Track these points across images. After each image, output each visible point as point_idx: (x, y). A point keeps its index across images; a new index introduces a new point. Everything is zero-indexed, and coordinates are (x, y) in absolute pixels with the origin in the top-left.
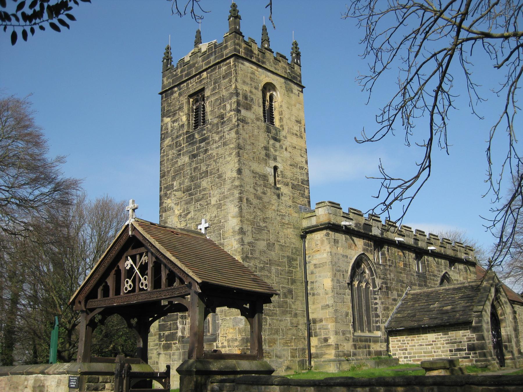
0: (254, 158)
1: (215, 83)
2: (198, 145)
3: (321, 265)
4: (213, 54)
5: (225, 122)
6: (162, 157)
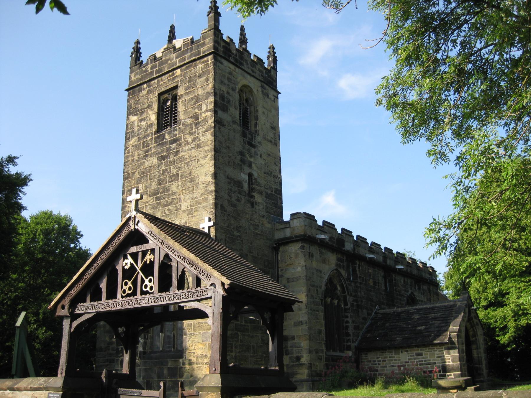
0: (229, 162)
1: (189, 82)
2: (168, 146)
3: (295, 280)
4: (189, 51)
5: (200, 123)
6: (126, 158)
